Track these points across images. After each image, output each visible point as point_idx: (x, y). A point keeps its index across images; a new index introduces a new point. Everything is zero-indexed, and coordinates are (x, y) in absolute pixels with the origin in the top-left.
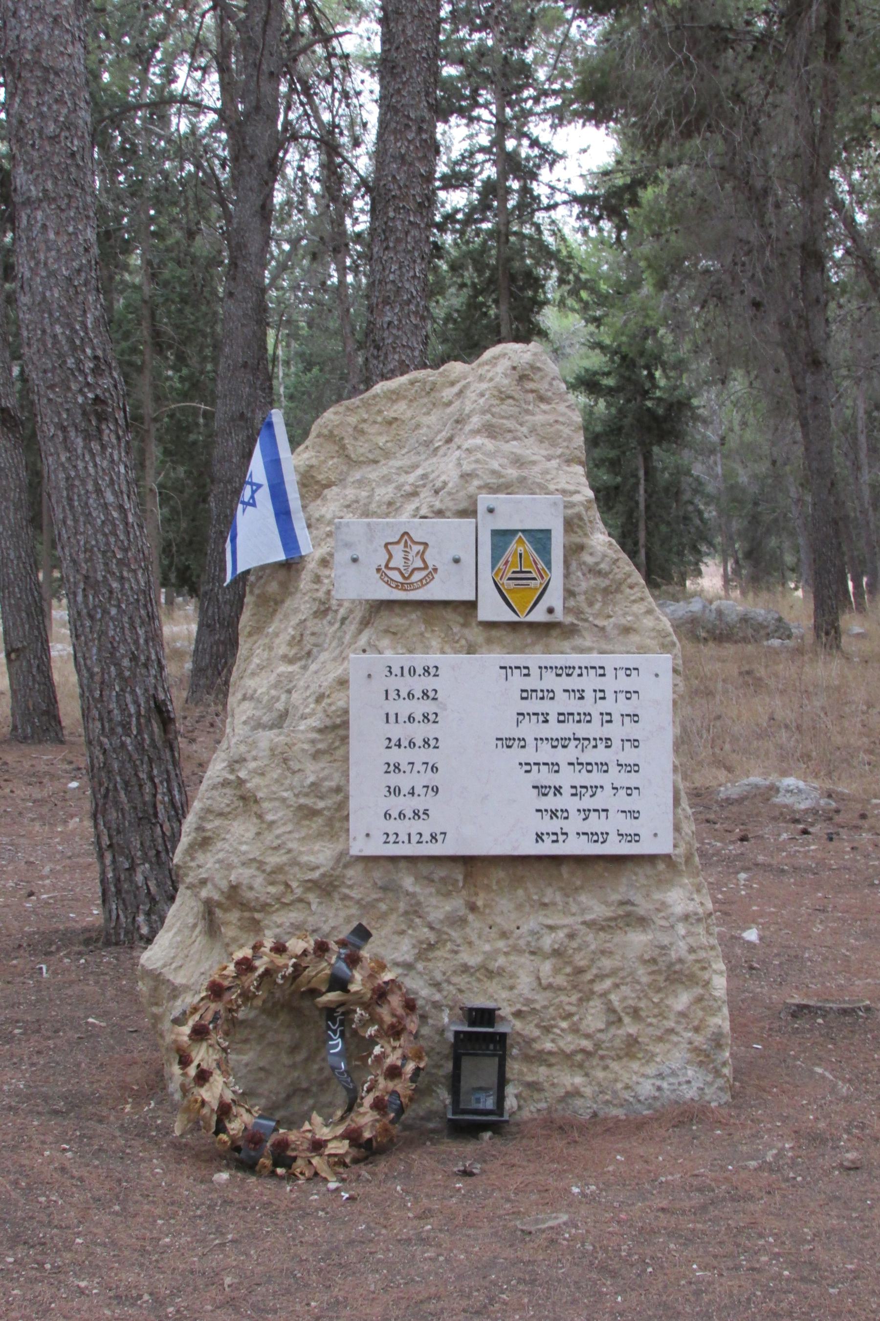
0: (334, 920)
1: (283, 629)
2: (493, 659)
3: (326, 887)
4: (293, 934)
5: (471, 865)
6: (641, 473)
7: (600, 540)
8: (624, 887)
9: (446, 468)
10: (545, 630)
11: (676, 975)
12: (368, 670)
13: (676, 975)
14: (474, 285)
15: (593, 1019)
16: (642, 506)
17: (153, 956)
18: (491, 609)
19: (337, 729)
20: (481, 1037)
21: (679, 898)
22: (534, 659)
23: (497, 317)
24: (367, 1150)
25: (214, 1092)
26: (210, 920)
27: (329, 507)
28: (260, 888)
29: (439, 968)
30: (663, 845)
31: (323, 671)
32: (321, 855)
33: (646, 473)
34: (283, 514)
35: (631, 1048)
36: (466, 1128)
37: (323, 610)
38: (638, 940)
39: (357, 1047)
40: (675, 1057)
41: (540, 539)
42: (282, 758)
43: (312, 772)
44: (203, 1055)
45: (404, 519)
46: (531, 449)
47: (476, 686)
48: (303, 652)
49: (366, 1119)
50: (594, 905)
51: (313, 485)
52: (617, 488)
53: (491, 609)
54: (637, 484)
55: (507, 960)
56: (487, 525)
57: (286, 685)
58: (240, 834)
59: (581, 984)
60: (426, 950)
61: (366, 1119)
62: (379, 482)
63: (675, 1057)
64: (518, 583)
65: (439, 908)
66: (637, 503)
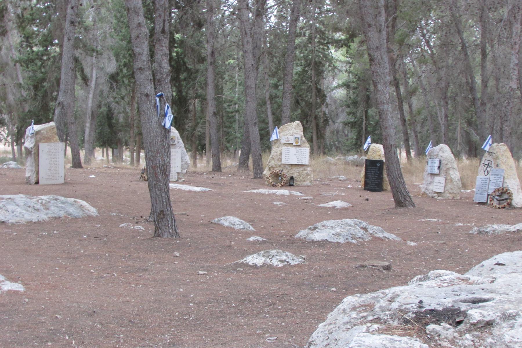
0: (280, 169)
1: (276, 145)
2: (294, 148)
3: (280, 166)
4: (277, 170)
5: (292, 165)
6: (364, 118)
7: (304, 138)
8: (304, 167)
9: (291, 132)
10: (299, 146)
11: (308, 175)
12: (284, 149)
13: (308, 175)
14: (305, 65)
15: (301, 178)
16: (364, 129)
17: (264, 173)
18: (294, 144)
19: (281, 153)
20: (292, 178)
21: (309, 168)
22: (298, 148)
23: (311, 74)
24: (282, 186)
25: (271, 181)
26: (270, 169)
27: (281, 134)
28: (274, 166)
29: (289, 173)
30: (307, 164)
31: (280, 149)
32: (279, 164)
33: (366, 118)
34: (277, 135)
35: (304, 181)
36: (290, 185)
37: (280, 144)
38: (305, 172)
39: (282, 179)
40: (308, 182)
41: (299, 138)
42: (276, 155)
43: (279, 157)
44: (270, 178)
45: (287, 136)
46: (298, 130)
47: (293, 150)
48: (278, 147)
49: (283, 183)
50: (302, 169)
51: (280, 133)
52: (355, 122)
53: (294, 144)
54: (362, 121)
55: (294, 172)
56: (294, 137)
57: (277, 150)
58: (273, 162)
59: (300, 175)
60: (288, 172)
61: (283, 183)
62: (285, 133)
63: (308, 182)
64: (297, 142)
65: (289, 168)
66: (362, 128)
